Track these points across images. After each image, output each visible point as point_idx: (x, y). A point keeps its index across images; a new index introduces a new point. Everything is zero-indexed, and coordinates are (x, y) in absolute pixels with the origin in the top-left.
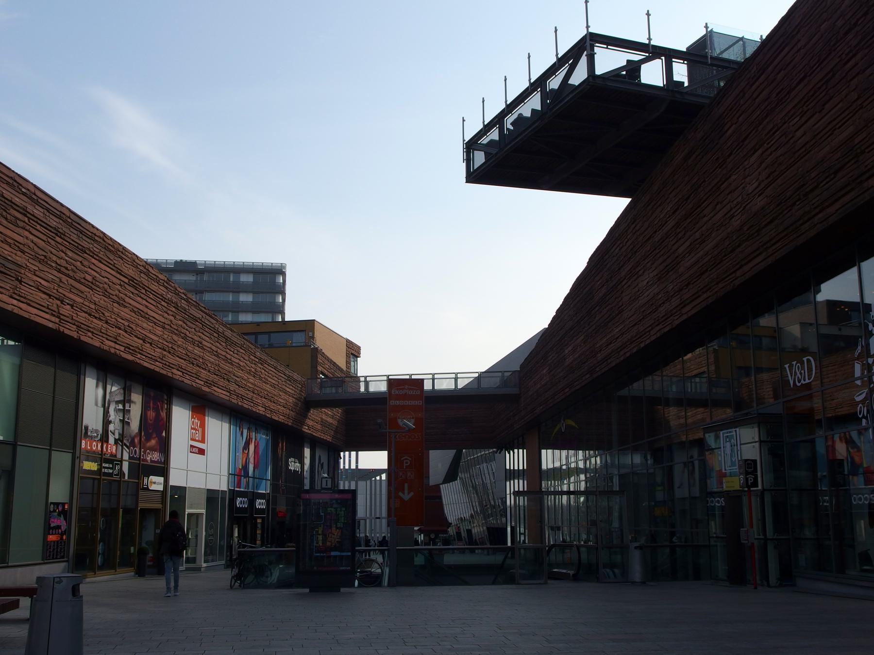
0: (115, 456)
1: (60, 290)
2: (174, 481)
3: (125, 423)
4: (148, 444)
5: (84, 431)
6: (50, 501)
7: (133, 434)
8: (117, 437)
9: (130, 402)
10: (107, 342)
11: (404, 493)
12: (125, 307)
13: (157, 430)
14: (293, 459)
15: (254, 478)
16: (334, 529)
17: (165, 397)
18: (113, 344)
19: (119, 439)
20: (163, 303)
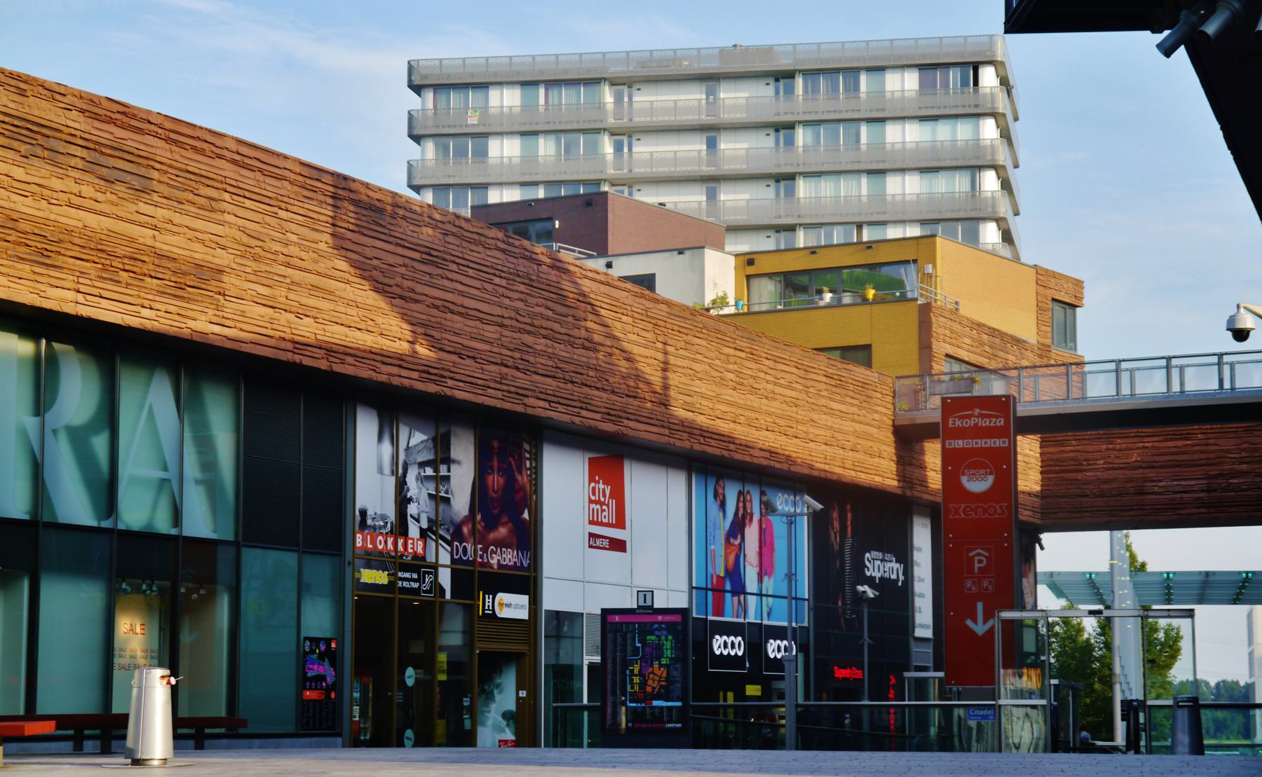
0: (423, 558)
1: (292, 296)
2: (551, 601)
3: (440, 500)
4: (492, 536)
5: (358, 518)
6: (303, 634)
7: (458, 518)
8: (425, 525)
9: (448, 461)
10: (384, 368)
11: (975, 622)
12: (417, 301)
13: (509, 509)
14: (875, 554)
15: (760, 595)
16: (656, 665)
17: (527, 447)
18: (395, 370)
19: (429, 529)
20: (497, 280)
